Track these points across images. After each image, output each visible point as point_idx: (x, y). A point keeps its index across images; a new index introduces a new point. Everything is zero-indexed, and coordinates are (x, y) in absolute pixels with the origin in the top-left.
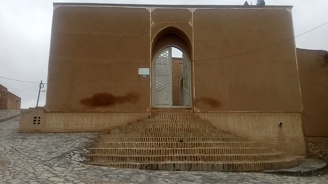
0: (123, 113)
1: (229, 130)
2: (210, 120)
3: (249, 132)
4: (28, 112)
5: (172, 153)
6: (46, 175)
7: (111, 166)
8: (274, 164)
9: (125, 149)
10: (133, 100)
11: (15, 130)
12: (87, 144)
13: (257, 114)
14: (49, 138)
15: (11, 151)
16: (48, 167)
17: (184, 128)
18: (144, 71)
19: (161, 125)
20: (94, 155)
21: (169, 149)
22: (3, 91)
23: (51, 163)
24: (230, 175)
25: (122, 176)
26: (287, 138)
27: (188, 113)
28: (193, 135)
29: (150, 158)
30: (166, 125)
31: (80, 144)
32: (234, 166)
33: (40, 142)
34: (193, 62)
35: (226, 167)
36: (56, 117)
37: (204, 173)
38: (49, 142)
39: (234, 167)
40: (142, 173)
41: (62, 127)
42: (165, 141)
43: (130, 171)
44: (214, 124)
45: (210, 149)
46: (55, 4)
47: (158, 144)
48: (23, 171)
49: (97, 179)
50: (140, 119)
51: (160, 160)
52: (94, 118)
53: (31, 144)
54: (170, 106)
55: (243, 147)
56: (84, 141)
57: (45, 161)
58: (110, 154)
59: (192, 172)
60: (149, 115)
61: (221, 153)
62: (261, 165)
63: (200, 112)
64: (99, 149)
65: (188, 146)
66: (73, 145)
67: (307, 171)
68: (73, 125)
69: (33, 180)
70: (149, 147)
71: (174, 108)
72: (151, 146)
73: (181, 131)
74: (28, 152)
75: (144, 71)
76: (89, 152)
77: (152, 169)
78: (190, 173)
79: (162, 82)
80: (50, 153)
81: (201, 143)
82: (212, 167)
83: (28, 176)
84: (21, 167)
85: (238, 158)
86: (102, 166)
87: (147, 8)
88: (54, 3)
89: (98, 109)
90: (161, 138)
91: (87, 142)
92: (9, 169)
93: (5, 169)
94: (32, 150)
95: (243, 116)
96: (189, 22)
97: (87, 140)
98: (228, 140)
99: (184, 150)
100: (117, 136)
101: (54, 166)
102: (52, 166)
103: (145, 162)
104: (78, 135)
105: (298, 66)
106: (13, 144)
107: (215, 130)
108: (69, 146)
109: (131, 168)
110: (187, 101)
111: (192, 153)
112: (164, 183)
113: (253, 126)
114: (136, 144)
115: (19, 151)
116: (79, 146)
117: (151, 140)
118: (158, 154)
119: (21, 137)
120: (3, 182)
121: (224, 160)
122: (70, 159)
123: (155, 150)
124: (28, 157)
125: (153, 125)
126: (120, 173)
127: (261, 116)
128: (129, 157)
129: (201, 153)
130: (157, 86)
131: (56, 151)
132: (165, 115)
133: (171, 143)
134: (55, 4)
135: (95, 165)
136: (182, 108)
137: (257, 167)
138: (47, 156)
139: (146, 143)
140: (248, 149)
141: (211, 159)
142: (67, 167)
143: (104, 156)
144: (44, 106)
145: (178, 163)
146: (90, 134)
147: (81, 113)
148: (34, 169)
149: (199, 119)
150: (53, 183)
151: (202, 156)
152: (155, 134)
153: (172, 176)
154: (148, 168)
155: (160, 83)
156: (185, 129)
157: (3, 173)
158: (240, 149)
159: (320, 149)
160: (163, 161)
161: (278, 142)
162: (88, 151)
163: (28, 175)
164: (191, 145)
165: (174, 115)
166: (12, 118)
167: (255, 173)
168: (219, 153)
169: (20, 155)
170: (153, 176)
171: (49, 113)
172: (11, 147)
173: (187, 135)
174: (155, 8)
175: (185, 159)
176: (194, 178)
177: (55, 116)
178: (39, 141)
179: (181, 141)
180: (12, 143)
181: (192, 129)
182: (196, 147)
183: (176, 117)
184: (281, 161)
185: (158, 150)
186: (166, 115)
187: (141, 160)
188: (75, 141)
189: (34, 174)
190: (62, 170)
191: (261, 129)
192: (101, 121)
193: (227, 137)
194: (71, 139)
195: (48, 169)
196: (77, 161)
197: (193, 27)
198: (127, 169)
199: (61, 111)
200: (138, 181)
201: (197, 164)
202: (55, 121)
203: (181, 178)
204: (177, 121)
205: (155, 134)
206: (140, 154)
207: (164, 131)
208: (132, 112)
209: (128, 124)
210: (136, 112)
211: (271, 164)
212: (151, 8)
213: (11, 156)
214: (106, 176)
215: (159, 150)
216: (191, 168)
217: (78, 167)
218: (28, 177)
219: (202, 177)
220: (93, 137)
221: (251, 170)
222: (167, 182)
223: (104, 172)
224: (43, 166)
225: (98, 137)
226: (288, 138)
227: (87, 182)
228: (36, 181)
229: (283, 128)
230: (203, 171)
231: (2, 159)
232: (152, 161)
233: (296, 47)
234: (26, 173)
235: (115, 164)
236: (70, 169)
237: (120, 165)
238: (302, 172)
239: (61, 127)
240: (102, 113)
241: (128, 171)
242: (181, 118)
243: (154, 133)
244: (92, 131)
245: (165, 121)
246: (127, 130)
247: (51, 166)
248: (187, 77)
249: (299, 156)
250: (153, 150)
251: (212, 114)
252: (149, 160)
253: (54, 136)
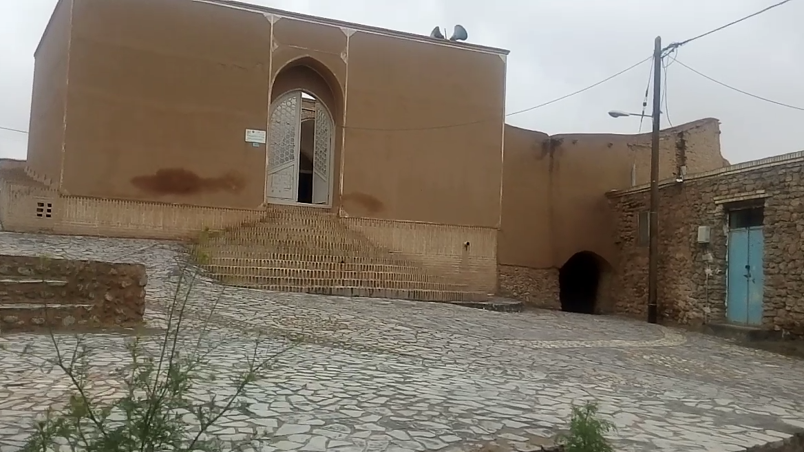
4: (26, 192)
10: (234, 187)
18: (255, 136)
19: (301, 236)
30: (309, 236)
34: (344, 130)
35: (412, 294)
36: (84, 207)
52: (161, 214)
68: (118, 223)
75: (255, 136)
87: (266, 14)
89: (168, 198)
174: (281, 16)
177: (83, 204)
233: (506, 123)
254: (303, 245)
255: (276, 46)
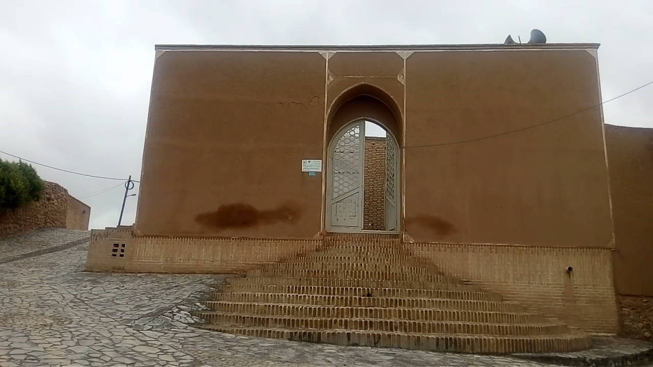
0: (271, 240)
1: (467, 277)
2: (432, 259)
3: (508, 283)
4: (105, 235)
5: (350, 316)
6: (129, 342)
7: (240, 333)
8: (536, 343)
9: (268, 304)
10: (290, 218)
11: (79, 267)
12: (202, 294)
13: (523, 250)
14: (138, 281)
15: (74, 302)
16: (134, 330)
17: (377, 272)
18: (311, 166)
19: (337, 265)
20: (213, 313)
21: (345, 308)
22: (60, 194)
23: (139, 324)
24: (446, 357)
25: (255, 349)
26: (580, 297)
27: (390, 244)
28: (393, 285)
29: (309, 322)
30: (345, 264)
31: (192, 294)
32: (458, 342)
33: (123, 288)
34: (404, 150)
35: (443, 345)
37: (398, 352)
38: (139, 288)
39: (458, 345)
40: (290, 347)
41: (162, 263)
42: (340, 294)
43: (271, 342)
44: (440, 265)
45: (418, 311)
46: (158, 47)
47: (327, 298)
48: (92, 335)
49: (214, 351)
50: (301, 252)
51: (326, 326)
52: (220, 248)
53: (108, 291)
54: (360, 230)
55: (486, 310)
56: (199, 289)
57: (129, 321)
58: (240, 313)
59: (379, 349)
60: (319, 247)
61: (439, 318)
62: (509, 344)
63: (413, 243)
64: (222, 304)
65: (380, 304)
66: (178, 295)
67: (598, 358)
68: (181, 259)
69: (109, 348)
70: (309, 304)
71: (366, 234)
72: (313, 302)
73: (371, 277)
74: (102, 305)
75: (311, 166)
76: (205, 309)
77: (309, 341)
78: (375, 350)
79: (346, 185)
80: (138, 307)
81: (404, 300)
82: (416, 342)
83: (101, 342)
84: (89, 327)
85: (468, 329)
86: (224, 332)
87: (321, 52)
88: (156, 46)
89: (227, 232)
90: (332, 288)
91: (203, 292)
92: (71, 330)
93: (64, 330)
94: (108, 301)
95: (496, 253)
96: (398, 76)
97: (203, 288)
98: (459, 295)
99: (371, 310)
100: (256, 282)
101: (145, 329)
102: (140, 328)
103: (300, 328)
104: (189, 278)
105: (608, 159)
106: (76, 291)
107: (437, 277)
108: (172, 296)
109: (273, 338)
110: (393, 222)
111: (386, 316)
112: (325, 363)
113: (515, 272)
114: (288, 297)
115: (86, 302)
116: (190, 298)
117: (355, 302)
118: (324, 316)
119: (90, 278)
120: (61, 349)
121: (442, 331)
122: (171, 319)
123: (319, 308)
124: (102, 314)
125: (322, 264)
126: (253, 345)
127: (532, 254)
128: (272, 319)
129: (402, 318)
130: (336, 192)
131: (150, 304)
132: (346, 247)
133: (349, 297)
134: (158, 47)
135: (214, 330)
136: (381, 234)
137: (501, 346)
138: (132, 312)
139: (305, 296)
140: (492, 315)
141: (419, 328)
142: (166, 331)
143: (230, 317)
144: (132, 225)
145: (356, 333)
146: (209, 277)
147: (197, 240)
148: (110, 332)
149: (411, 255)
150: (141, 354)
151: (401, 323)
152: (324, 281)
153: (341, 354)
154: (303, 339)
155: (341, 187)
156: (379, 273)
157: (60, 336)
158: (475, 313)
159: (646, 320)
160: (331, 327)
161: (564, 305)
162: (203, 307)
163: (102, 341)
164: (385, 303)
165: (362, 247)
166: (74, 244)
167: (496, 357)
168: (434, 319)
169: (87, 309)
170: (308, 352)
171: (141, 237)
172: (73, 294)
173: (381, 284)
174: (335, 52)
175: (371, 327)
176: (379, 358)
177: (151, 244)
178: (122, 286)
179: (369, 295)
180: (75, 289)
181: (393, 273)
182: (394, 306)
183: (368, 251)
184: (551, 338)
185: (324, 309)
186: (348, 247)
187: (293, 326)
188: (183, 289)
189: (111, 340)
190: (156, 335)
191: (531, 278)
192: (231, 255)
193: (457, 292)
194: (176, 285)
195: (133, 333)
196: (183, 323)
197: (405, 85)
198: (267, 339)
199: (161, 235)
200: (280, 358)
201: (389, 336)
202: (150, 252)
203: (356, 358)
204: (368, 259)
205: (324, 281)
206: (293, 315)
207: (340, 276)
208: (288, 240)
209: (280, 262)
210: (296, 240)
211: (529, 342)
212: (329, 52)
213: (74, 311)
214: (229, 348)
215: (326, 309)
216: (378, 341)
217: (183, 332)
218: (100, 344)
219: (393, 358)
220: (215, 283)
221: (489, 350)
222: (329, 362)
223: (227, 343)
224: (125, 328)
225: (224, 282)
226: (583, 297)
227: (196, 356)
228: (113, 350)
229: (573, 277)
230: (401, 348)
231: (59, 314)
232: (312, 327)
234: (97, 338)
235: (247, 330)
236: (171, 334)
237: (255, 332)
238: (588, 360)
239: (160, 262)
240: (233, 239)
241: (268, 343)
242: (376, 254)
243: (322, 279)
244: (214, 272)
245: (345, 258)
246: (275, 271)
247: (138, 329)
248: (393, 176)
249: (604, 332)
250: (315, 309)
251: (437, 247)
252: (306, 325)
253: (146, 279)
254: (333, 275)
255: (331, 79)
